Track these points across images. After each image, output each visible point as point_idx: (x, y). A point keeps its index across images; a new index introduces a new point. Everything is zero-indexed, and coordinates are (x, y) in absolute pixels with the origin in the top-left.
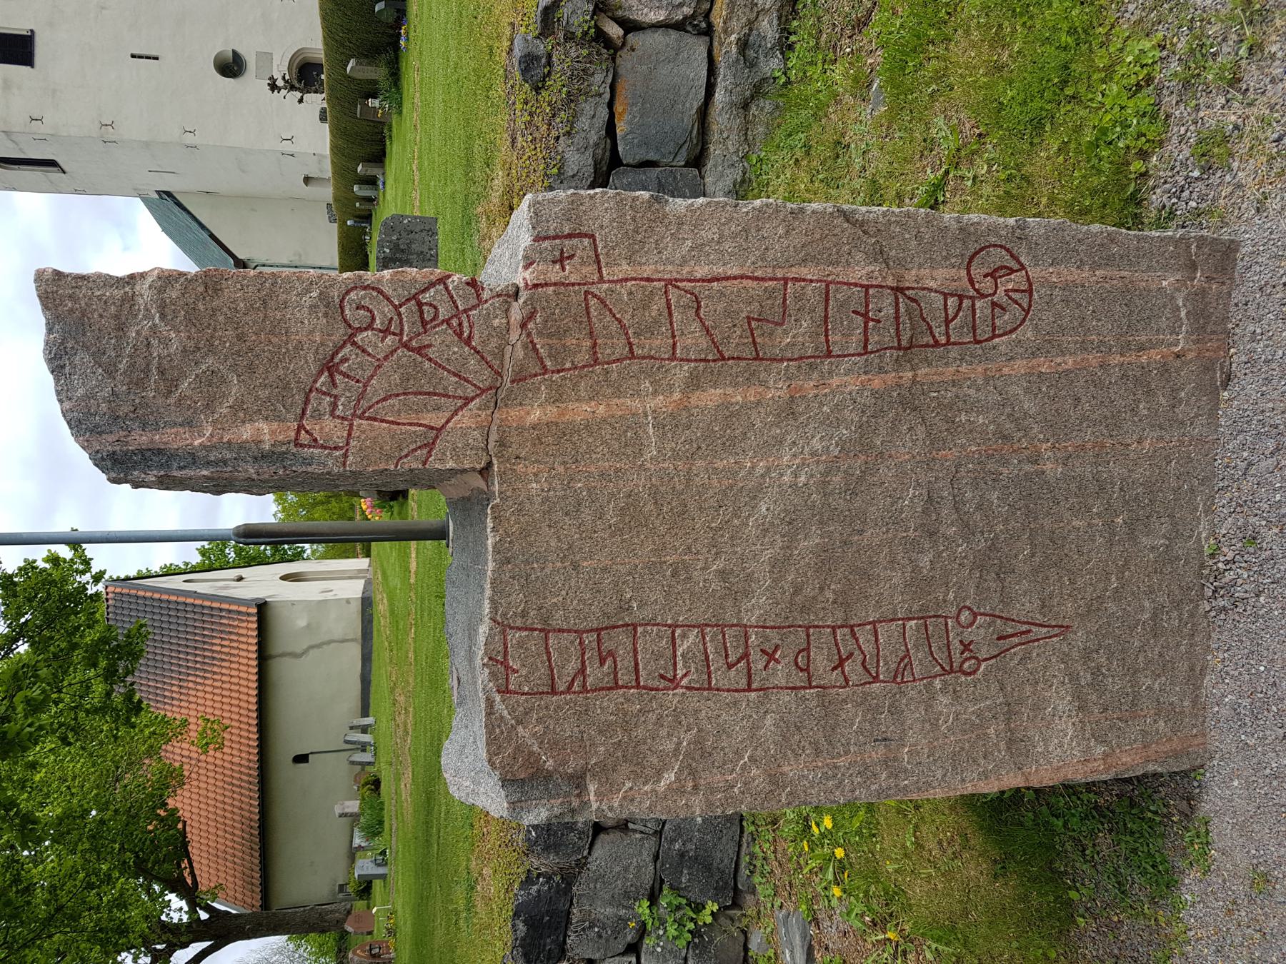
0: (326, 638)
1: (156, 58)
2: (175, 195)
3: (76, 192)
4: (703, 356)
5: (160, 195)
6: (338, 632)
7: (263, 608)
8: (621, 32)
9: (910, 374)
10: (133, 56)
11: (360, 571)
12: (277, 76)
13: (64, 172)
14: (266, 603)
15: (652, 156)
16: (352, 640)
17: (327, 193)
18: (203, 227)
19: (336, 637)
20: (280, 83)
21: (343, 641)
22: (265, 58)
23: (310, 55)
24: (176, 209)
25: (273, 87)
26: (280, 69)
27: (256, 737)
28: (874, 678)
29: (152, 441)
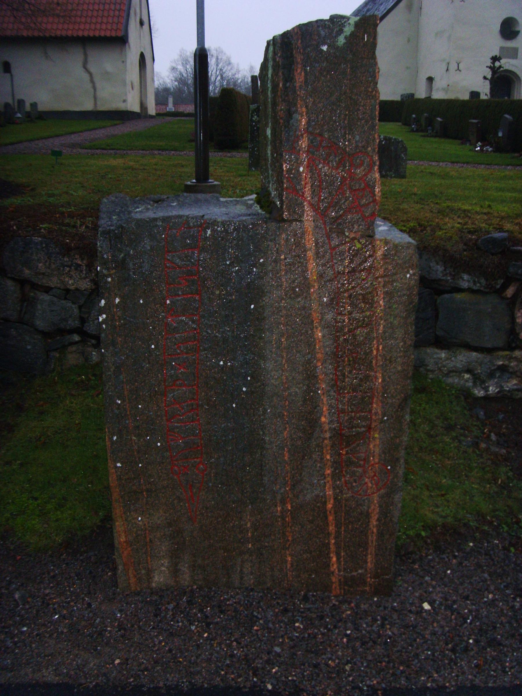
0: (98, 85)
6: (100, 94)
8: (509, 296)
11: (146, 109)
12: (503, 61)
16: (95, 104)
17: (421, 94)
19: (98, 93)
20: (497, 64)
21: (95, 98)
22: (513, 53)
23: (516, 87)
25: (495, 59)
26: (506, 64)
29: (297, 63)
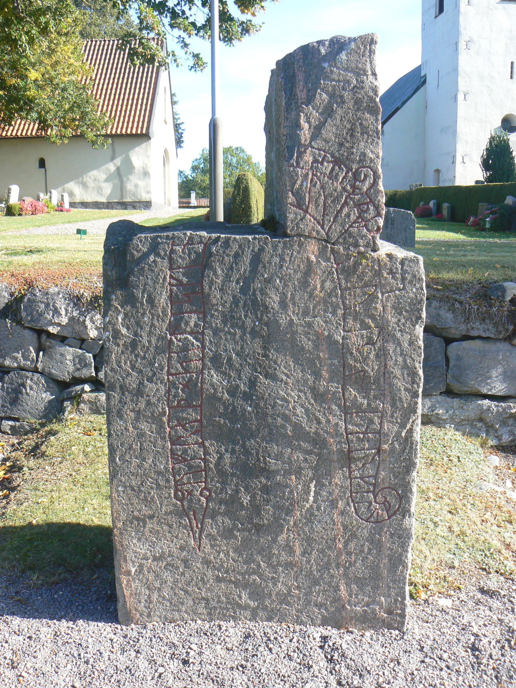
1: (511, 77)
2: (424, 87)
3: (423, 25)
4: (345, 346)
5: (423, 76)
6: (129, 187)
7: (145, 136)
9: (335, 458)
10: (512, 63)
13: (436, 17)
14: (150, 138)
15: (452, 363)
18: (404, 103)
24: (415, 87)
27: (19, 134)
28: (174, 441)
